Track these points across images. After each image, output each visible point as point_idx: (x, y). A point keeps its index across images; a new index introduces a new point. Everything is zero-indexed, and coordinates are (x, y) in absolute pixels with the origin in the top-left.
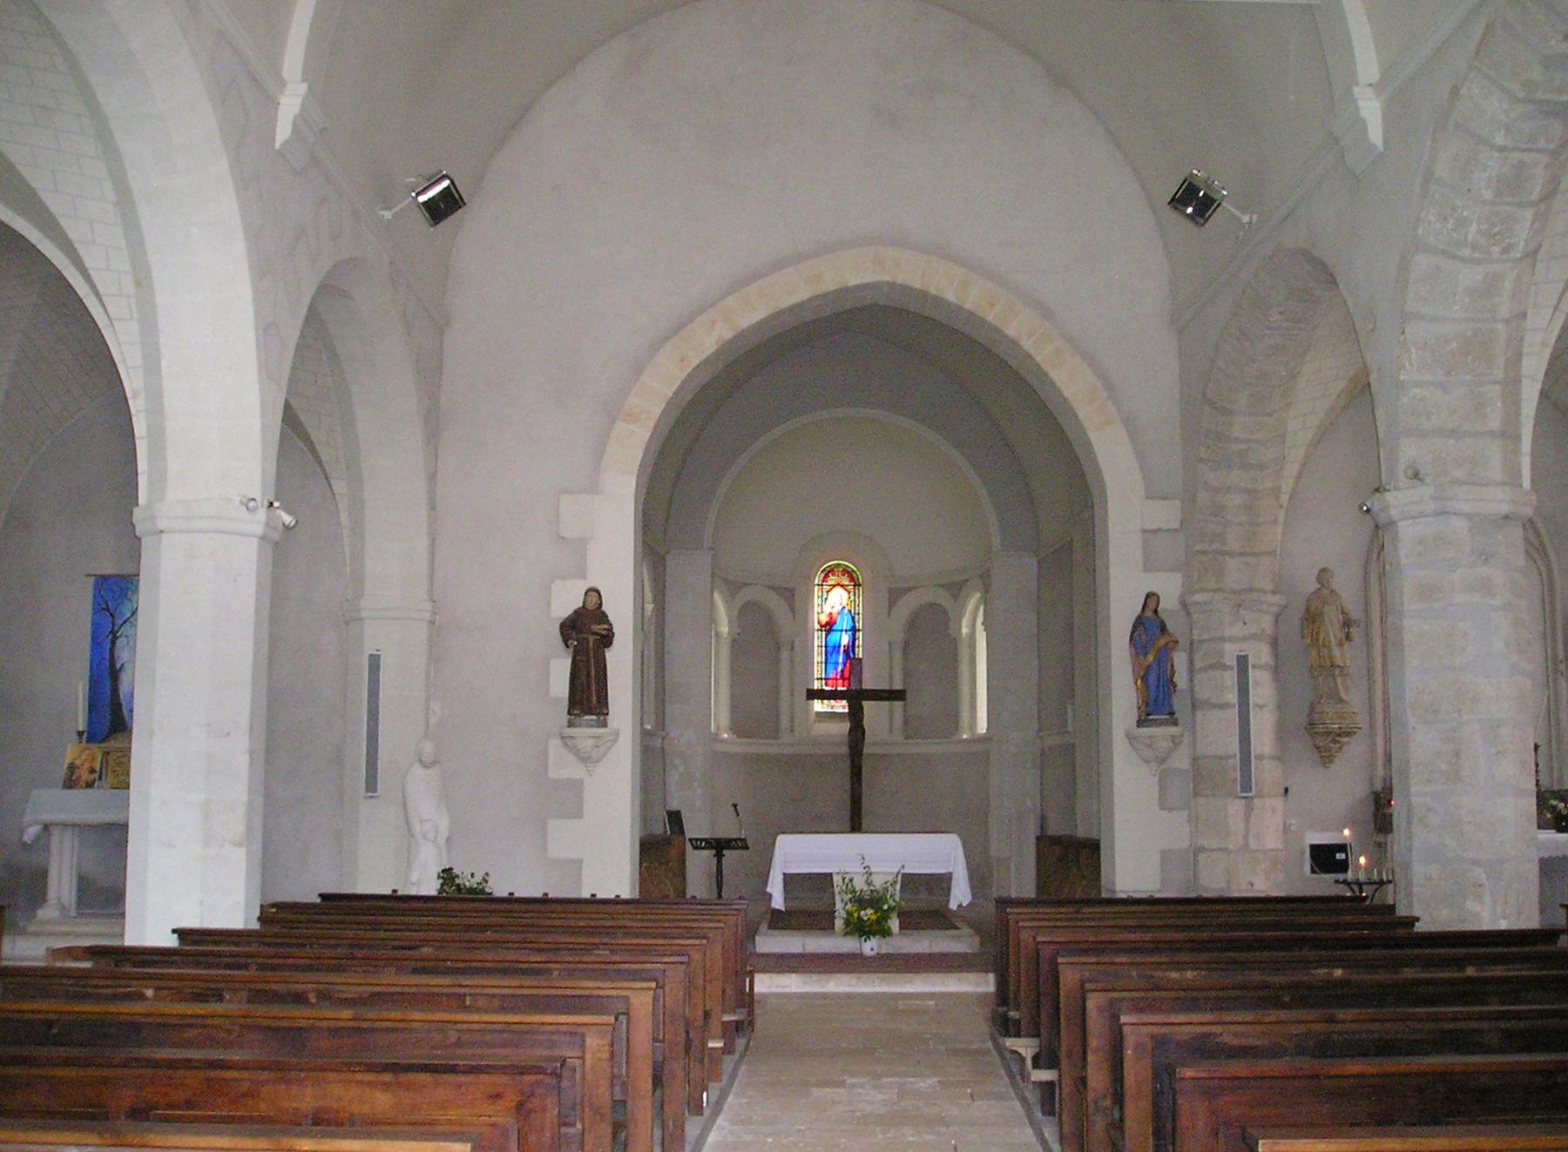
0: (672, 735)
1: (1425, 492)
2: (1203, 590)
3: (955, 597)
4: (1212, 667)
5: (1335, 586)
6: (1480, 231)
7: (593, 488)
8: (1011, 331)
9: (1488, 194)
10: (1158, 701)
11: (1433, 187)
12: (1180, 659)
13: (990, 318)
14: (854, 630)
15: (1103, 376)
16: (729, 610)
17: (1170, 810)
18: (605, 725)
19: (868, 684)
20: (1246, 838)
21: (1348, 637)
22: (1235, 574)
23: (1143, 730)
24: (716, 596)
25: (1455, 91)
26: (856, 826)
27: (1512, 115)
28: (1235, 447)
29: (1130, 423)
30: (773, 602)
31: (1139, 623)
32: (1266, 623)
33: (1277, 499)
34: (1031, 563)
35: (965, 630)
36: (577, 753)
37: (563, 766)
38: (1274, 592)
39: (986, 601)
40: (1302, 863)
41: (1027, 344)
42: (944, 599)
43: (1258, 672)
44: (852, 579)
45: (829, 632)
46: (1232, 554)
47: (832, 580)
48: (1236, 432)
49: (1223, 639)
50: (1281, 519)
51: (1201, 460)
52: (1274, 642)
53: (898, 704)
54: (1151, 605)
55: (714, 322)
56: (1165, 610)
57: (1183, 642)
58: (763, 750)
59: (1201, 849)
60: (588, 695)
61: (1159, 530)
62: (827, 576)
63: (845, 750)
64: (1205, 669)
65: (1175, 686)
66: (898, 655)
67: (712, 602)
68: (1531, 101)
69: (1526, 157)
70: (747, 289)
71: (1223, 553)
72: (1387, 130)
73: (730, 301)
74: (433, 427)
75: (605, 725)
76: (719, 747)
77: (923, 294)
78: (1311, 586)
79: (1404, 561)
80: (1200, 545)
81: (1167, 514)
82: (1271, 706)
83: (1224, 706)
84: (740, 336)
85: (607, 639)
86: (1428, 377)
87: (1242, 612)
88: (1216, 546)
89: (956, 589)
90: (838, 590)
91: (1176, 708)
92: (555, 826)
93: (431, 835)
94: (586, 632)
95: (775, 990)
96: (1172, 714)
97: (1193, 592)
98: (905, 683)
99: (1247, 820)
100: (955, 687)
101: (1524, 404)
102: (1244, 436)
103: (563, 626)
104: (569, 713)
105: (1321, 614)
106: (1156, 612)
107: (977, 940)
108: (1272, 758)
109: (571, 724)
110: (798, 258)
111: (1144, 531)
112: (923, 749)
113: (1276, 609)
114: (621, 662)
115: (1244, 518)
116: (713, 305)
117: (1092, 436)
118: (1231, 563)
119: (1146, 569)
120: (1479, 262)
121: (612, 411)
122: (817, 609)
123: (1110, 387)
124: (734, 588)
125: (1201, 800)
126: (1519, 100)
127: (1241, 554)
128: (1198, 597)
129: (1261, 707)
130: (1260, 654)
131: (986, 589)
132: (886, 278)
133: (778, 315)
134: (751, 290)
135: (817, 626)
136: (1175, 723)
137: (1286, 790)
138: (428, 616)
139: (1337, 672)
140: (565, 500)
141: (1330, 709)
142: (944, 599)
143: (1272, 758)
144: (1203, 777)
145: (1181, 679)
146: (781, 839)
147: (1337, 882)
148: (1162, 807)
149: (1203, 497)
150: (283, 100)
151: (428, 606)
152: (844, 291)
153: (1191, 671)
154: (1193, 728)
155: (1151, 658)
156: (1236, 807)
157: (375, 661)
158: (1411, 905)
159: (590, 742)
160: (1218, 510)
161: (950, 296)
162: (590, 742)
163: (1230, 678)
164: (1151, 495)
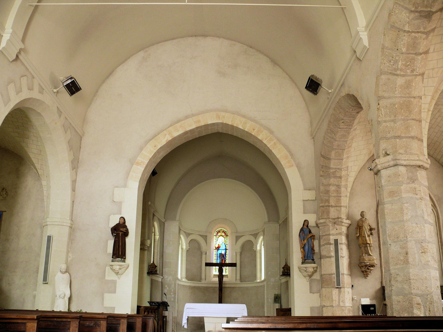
1: (389, 158)
3: (256, 238)
6: (402, 64)
7: (125, 186)
8: (260, 137)
9: (404, 50)
10: (309, 255)
11: (385, 50)
12: (316, 243)
13: (253, 134)
14: (226, 249)
15: (290, 152)
16: (186, 241)
17: (313, 293)
20: (339, 302)
21: (371, 234)
22: (333, 213)
23: (303, 265)
24: (181, 236)
25: (390, 15)
27: (410, 18)
29: (299, 167)
30: (201, 241)
31: (302, 230)
33: (346, 189)
34: (277, 225)
36: (113, 270)
37: (110, 276)
38: (346, 219)
40: (359, 311)
41: (265, 142)
42: (252, 238)
44: (225, 234)
45: (218, 250)
46: (332, 206)
47: (219, 234)
49: (329, 235)
51: (321, 176)
55: (166, 135)
57: (316, 237)
58: (197, 285)
59: (324, 306)
60: (119, 252)
62: (218, 233)
64: (324, 245)
65: (314, 251)
67: (180, 238)
68: (417, 12)
69: (417, 35)
70: (177, 125)
71: (329, 206)
72: (370, 37)
73: (171, 128)
74: (75, 165)
77: (232, 126)
79: (383, 184)
80: (323, 202)
83: (330, 257)
84: (174, 139)
85: (126, 234)
86: (388, 119)
87: (336, 226)
88: (327, 204)
89: (256, 236)
91: (315, 258)
92: (107, 296)
93: (62, 296)
94: (120, 232)
96: (313, 260)
97: (320, 219)
99: (339, 296)
100: (255, 266)
101: (423, 130)
102: (335, 167)
103: (112, 229)
104: (112, 258)
105: (362, 226)
106: (307, 226)
108: (346, 275)
109: (112, 261)
110: (193, 115)
111: (303, 200)
112: (246, 285)
115: (335, 194)
116: (166, 129)
117: (286, 170)
119: (304, 213)
120: (404, 76)
121: (133, 162)
122: (214, 243)
123: (292, 155)
124: (188, 235)
125: (323, 289)
126: (412, 11)
127: (334, 207)
128: (322, 221)
130: (343, 240)
131: (264, 235)
132: (220, 121)
133: (186, 133)
134: (178, 125)
135: (214, 248)
137: (353, 286)
138: (69, 225)
139: (368, 245)
140: (116, 189)
141: (366, 257)
142: (252, 238)
144: (324, 282)
148: (311, 292)
149: (322, 188)
150: (4, 35)
151: (69, 222)
152: (206, 126)
153: (320, 246)
154: (320, 265)
155: (306, 241)
156: (335, 292)
158: (393, 313)
159: (118, 267)
160: (327, 192)
161: (240, 127)
162: (118, 267)
163: (332, 248)
164: (305, 189)
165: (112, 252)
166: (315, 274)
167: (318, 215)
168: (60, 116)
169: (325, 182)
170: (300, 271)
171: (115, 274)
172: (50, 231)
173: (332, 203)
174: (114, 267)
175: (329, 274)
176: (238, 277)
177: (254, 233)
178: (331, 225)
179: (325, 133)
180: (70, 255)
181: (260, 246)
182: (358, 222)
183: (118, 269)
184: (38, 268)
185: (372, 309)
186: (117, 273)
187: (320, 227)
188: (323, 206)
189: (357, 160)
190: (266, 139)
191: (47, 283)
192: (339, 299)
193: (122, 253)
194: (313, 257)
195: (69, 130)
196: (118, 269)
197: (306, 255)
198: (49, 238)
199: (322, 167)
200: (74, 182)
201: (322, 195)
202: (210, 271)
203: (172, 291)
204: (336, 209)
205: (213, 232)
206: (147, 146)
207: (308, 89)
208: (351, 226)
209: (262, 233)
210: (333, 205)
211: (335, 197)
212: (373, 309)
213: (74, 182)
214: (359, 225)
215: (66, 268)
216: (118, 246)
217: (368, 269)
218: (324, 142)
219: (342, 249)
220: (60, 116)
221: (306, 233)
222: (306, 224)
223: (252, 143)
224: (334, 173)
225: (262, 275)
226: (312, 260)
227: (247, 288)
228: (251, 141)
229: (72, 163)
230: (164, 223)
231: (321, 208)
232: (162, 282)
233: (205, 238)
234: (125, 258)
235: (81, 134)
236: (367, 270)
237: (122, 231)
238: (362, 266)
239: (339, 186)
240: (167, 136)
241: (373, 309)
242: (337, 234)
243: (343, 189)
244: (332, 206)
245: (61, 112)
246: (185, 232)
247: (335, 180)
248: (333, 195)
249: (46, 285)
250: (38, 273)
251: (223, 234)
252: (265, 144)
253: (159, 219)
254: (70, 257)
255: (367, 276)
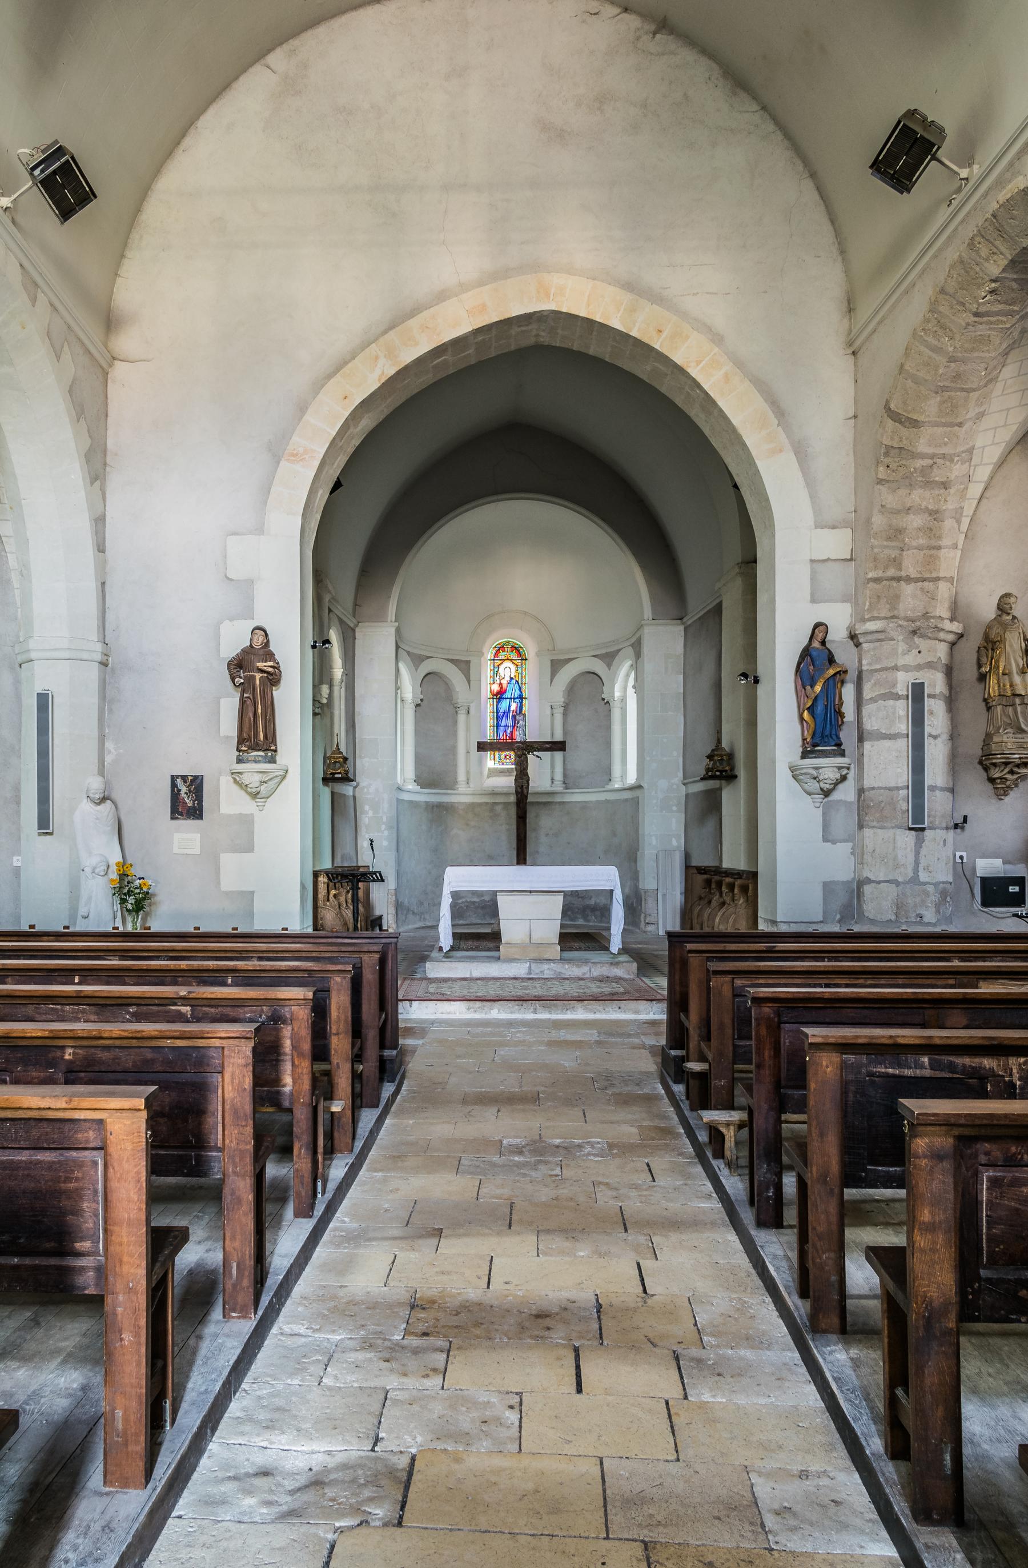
0: (362, 785)
2: (873, 619)
4: (885, 697)
5: (1015, 612)
12: (848, 692)
17: (834, 842)
18: (273, 760)
19: (532, 735)
20: (916, 870)
24: (401, 665)
26: (521, 859)
28: (919, 463)
31: (806, 653)
32: (941, 651)
35: (617, 694)
39: (636, 667)
43: (932, 701)
44: (519, 654)
46: (908, 580)
47: (502, 655)
48: (922, 446)
50: (960, 546)
51: (880, 482)
52: (949, 672)
53: (558, 755)
54: (820, 635)
55: (377, 358)
56: (833, 641)
59: (868, 881)
61: (828, 559)
62: (498, 652)
63: (513, 799)
64: (874, 700)
66: (559, 717)
71: (898, 579)
74: (97, 463)
75: (273, 760)
76: (406, 797)
78: (989, 612)
80: (882, 565)
81: (836, 544)
82: (945, 737)
85: (273, 678)
87: (917, 640)
88: (891, 572)
89: (609, 658)
90: (507, 664)
94: (252, 672)
95: (439, 1016)
96: (839, 745)
97: (864, 621)
98: (565, 733)
102: (930, 450)
104: (238, 750)
105: (1003, 641)
106: (823, 643)
107: (635, 965)
108: (942, 789)
109: (239, 761)
111: (811, 561)
113: (951, 637)
114: (291, 703)
115: (922, 541)
116: (375, 340)
118: (908, 590)
121: (277, 452)
124: (417, 660)
125: (867, 832)
127: (917, 580)
128: (871, 626)
129: (935, 737)
130: (936, 683)
131: (638, 655)
135: (489, 695)
136: (843, 754)
138: (99, 657)
140: (232, 540)
142: (598, 666)
143: (942, 789)
145: (849, 709)
146: (449, 870)
147: (1016, 915)
148: (825, 840)
149: (878, 521)
151: (99, 647)
155: (818, 688)
157: (44, 702)
159: (257, 778)
160: (896, 533)
162: (257, 778)
163: (902, 709)
165: (234, 733)
166: (840, 786)
167: (856, 604)
168: (34, 300)
169: (889, 498)
170: (794, 777)
171: (248, 797)
172: (43, 677)
173: (910, 568)
174: (246, 779)
175: (890, 789)
176: (559, 776)
177: (603, 651)
178: (901, 638)
179: (914, 334)
180: (109, 745)
181: (623, 687)
182: (989, 627)
183: (257, 784)
184: (17, 789)
185: (1014, 889)
186: (255, 795)
187: (864, 645)
188: (876, 580)
189: (1005, 425)
190: (698, 363)
191: (51, 834)
192: (917, 862)
193: (266, 737)
194: (838, 738)
195: (66, 348)
196: (257, 784)
197: (819, 730)
198: (44, 702)
199: (888, 450)
200: (99, 522)
201: (876, 543)
202: (481, 762)
203: (385, 819)
204: (922, 589)
205: (485, 650)
206: (320, 395)
207: (878, 170)
208: (964, 639)
209: (630, 651)
210: (913, 573)
211: (919, 548)
212: (1017, 889)
213: (99, 522)
214: (992, 636)
215: (102, 786)
216: (251, 715)
217: (1012, 772)
218: (907, 367)
219: (931, 713)
220: (34, 300)
221: (817, 663)
222: (820, 635)
223: (645, 378)
224: (924, 471)
225: (627, 770)
226: (835, 745)
227: (584, 806)
228: (643, 371)
229: (88, 461)
230: (354, 631)
231: (871, 585)
232: (354, 797)
233: (464, 666)
234: (275, 751)
235: (105, 365)
236: (1009, 776)
237: (262, 671)
238: (995, 765)
239: (935, 515)
240: (382, 361)
241: (1017, 889)
242: (919, 667)
243: (949, 523)
244: (908, 580)
245: (36, 285)
246: (409, 653)
247: (927, 494)
248: (914, 543)
249: (48, 837)
250: (18, 803)
251: (514, 655)
252: (694, 380)
253: (341, 622)
254: (110, 752)
255: (1006, 795)
